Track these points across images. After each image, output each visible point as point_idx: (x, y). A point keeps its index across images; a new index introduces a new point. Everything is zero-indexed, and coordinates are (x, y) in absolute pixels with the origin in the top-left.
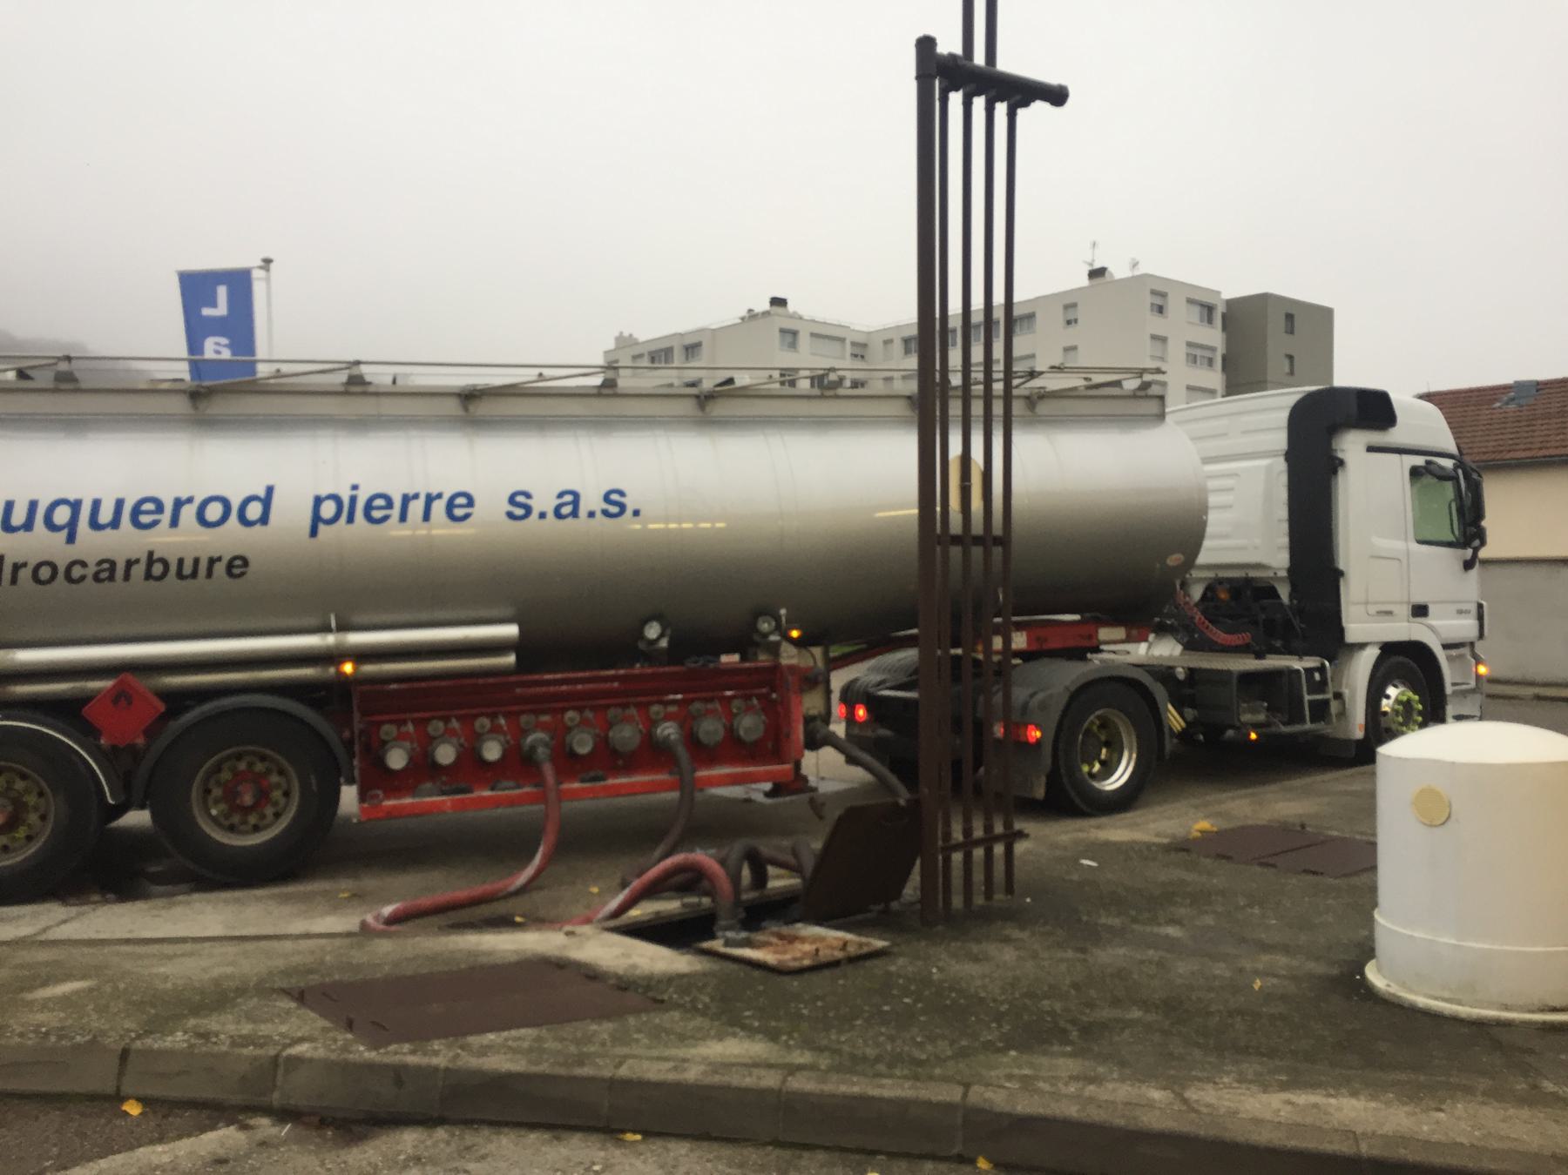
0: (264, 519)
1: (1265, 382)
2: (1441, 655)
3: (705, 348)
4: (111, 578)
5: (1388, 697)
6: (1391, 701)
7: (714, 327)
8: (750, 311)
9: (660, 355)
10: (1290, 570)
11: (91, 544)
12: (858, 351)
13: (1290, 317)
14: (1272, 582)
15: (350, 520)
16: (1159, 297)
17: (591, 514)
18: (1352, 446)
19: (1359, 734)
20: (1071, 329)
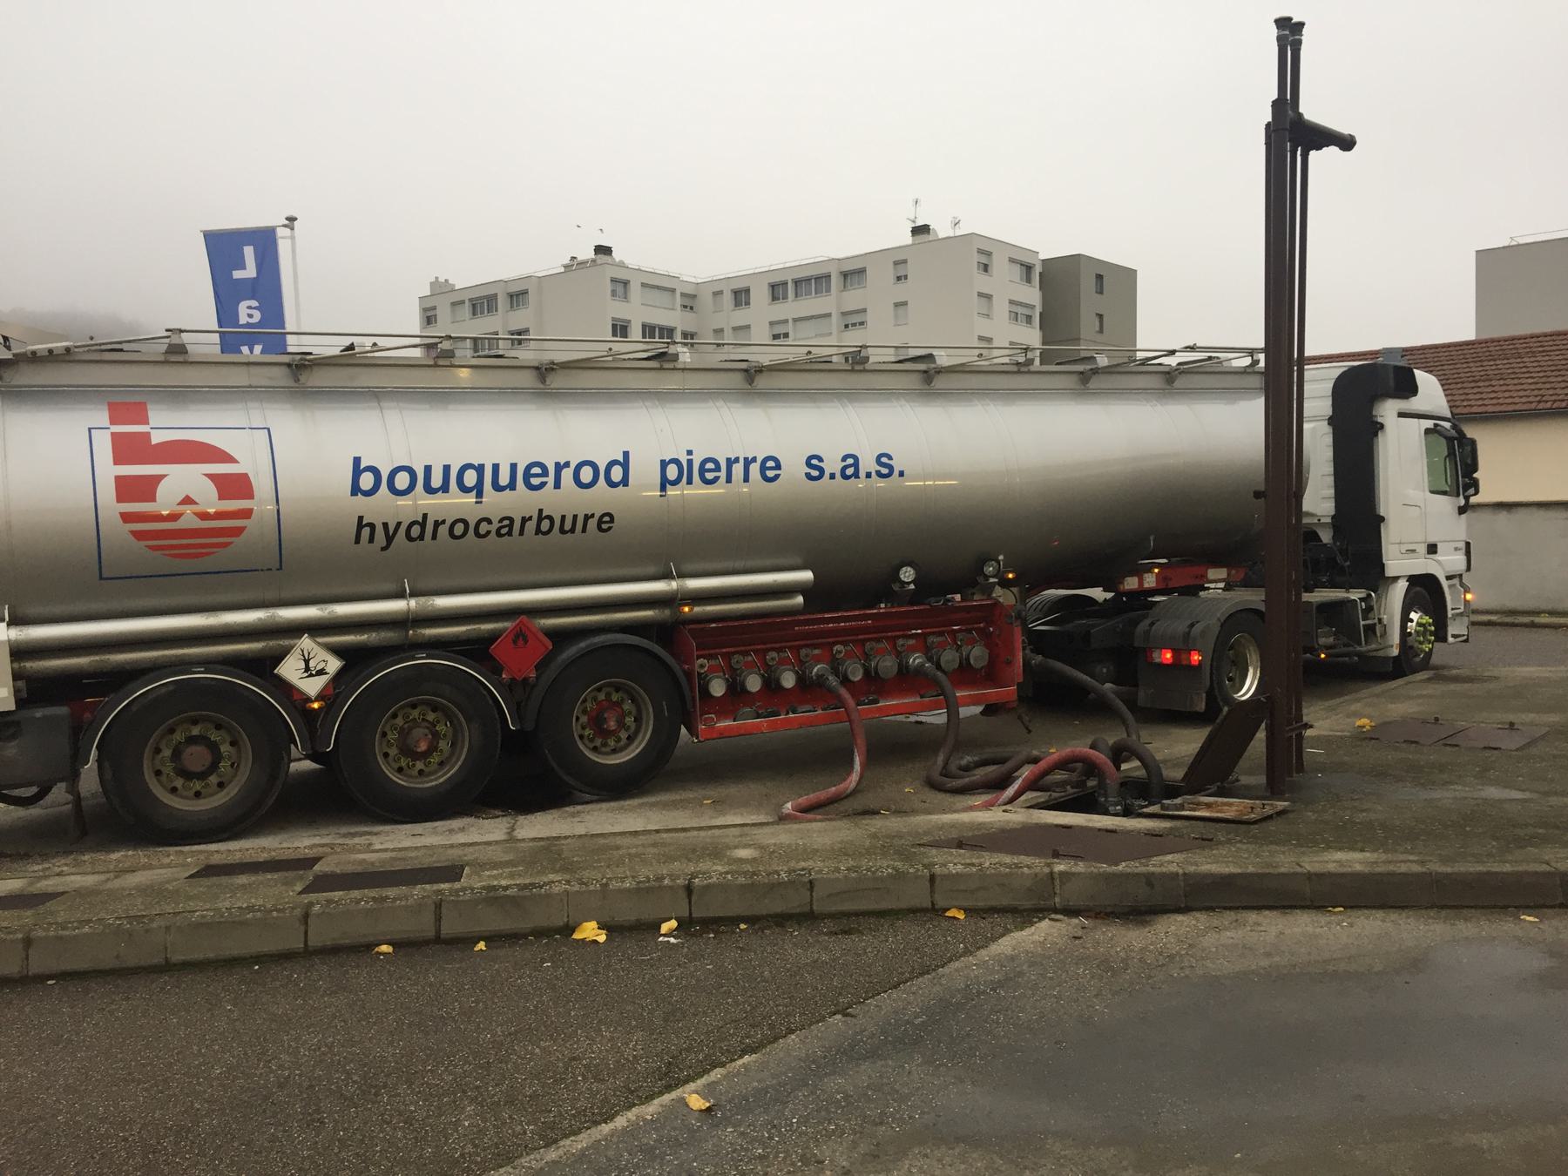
0: (625, 481)
1: (1079, 339)
2: (1445, 584)
3: (532, 297)
4: (510, 533)
5: (1412, 621)
6: (1414, 624)
7: (540, 275)
8: (573, 258)
9: (482, 303)
10: (1333, 517)
11: (496, 503)
12: (688, 302)
13: (1100, 277)
14: (1315, 528)
15: (690, 482)
16: (984, 254)
17: (868, 475)
18: (1388, 411)
19: (1395, 652)
20: (902, 285)
